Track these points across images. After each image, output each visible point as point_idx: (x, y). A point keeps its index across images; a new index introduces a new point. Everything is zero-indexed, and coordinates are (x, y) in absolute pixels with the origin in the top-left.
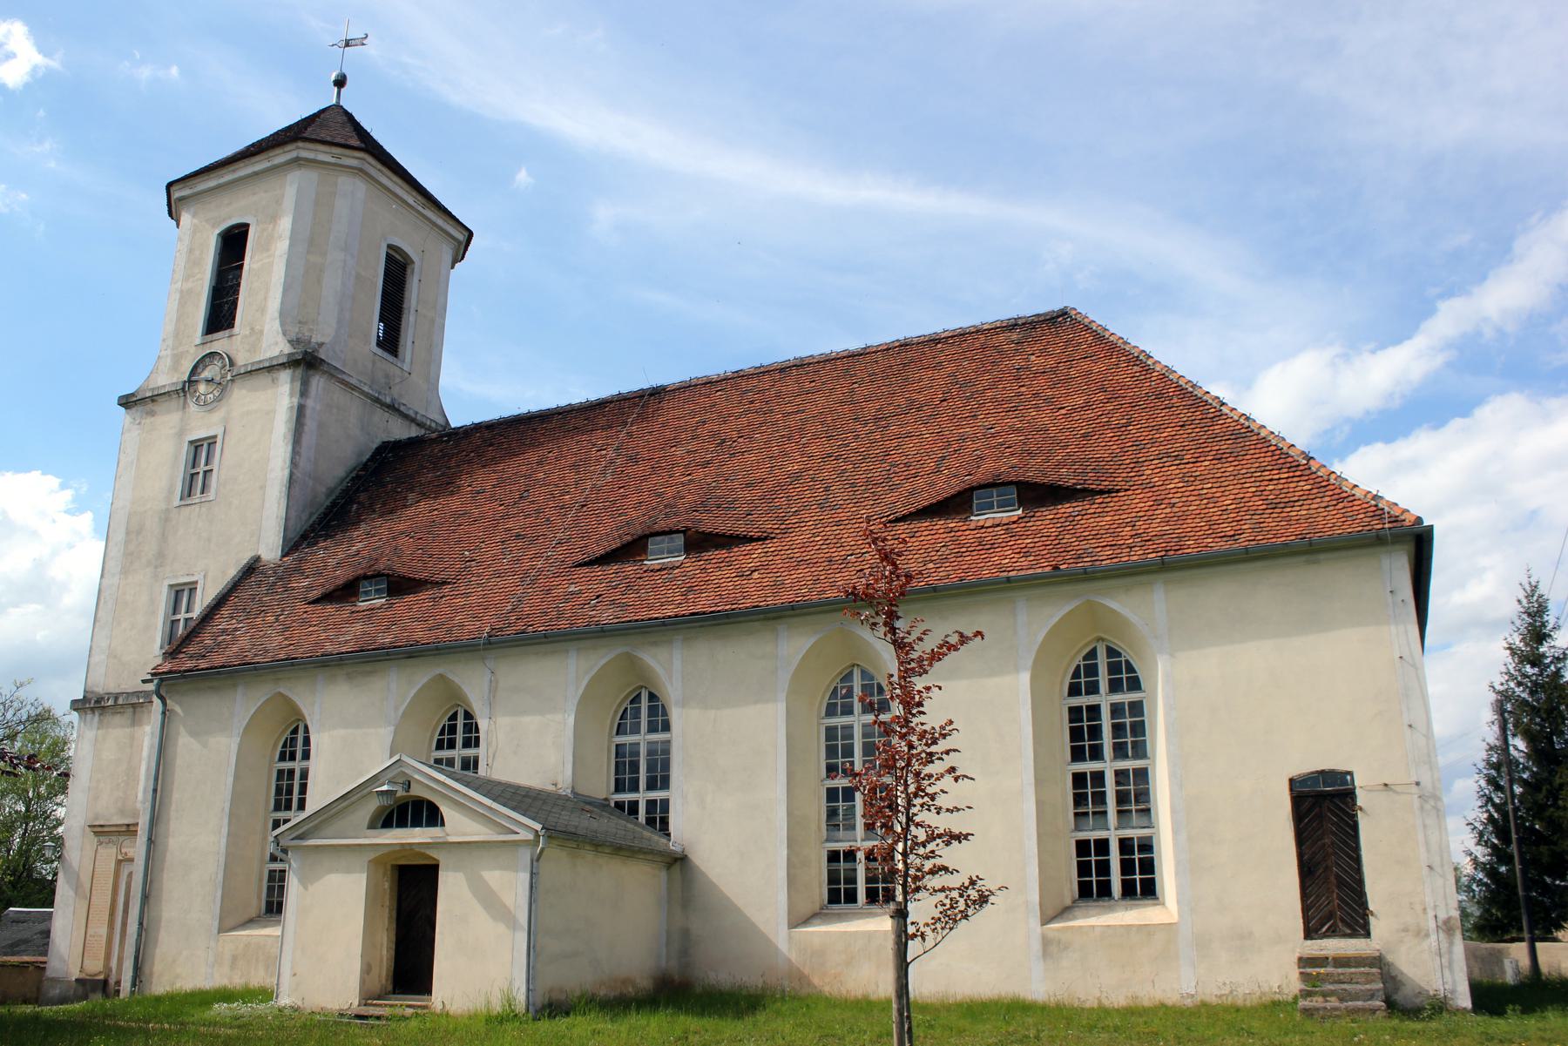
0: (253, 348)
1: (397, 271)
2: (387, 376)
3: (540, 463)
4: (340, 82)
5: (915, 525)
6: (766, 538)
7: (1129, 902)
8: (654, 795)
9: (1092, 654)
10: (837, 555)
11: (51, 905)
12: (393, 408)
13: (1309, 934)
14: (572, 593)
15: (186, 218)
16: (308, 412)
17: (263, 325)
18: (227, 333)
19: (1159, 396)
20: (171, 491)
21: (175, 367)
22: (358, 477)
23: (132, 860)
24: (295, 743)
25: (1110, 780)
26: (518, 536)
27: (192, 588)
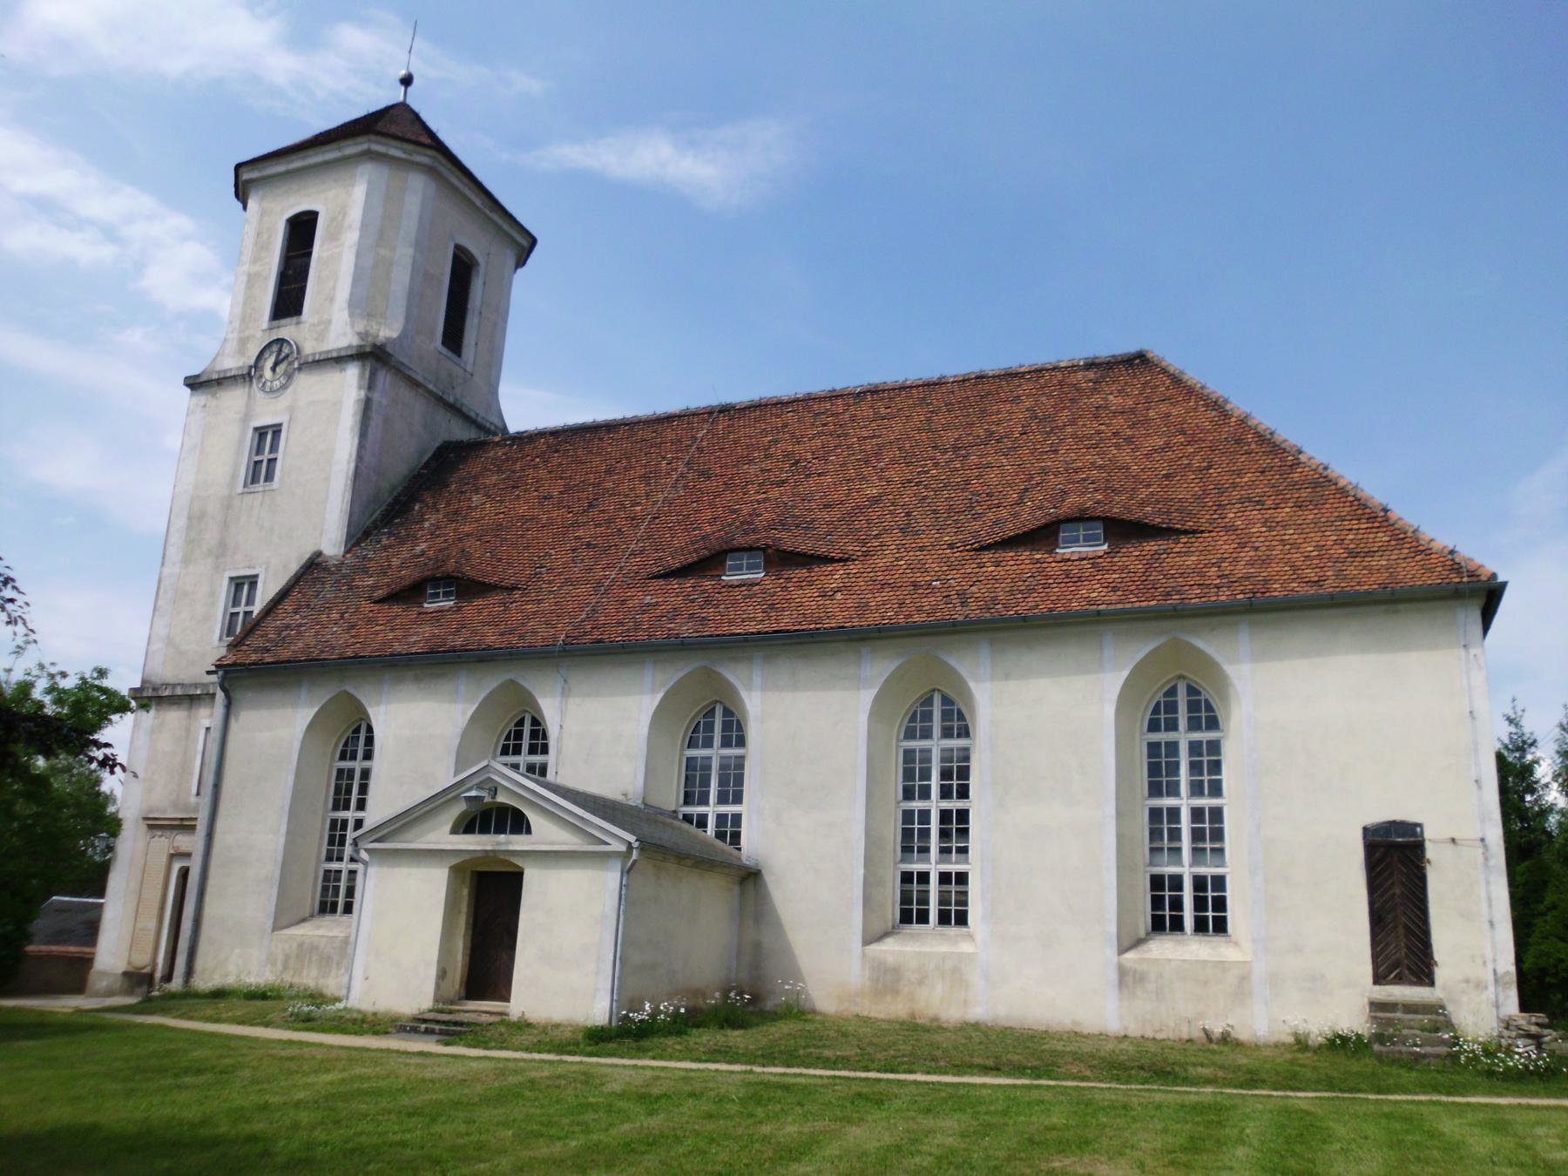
0: (321, 336)
1: (463, 269)
2: (450, 375)
3: (609, 472)
4: (407, 81)
5: (1000, 555)
6: (847, 560)
7: (1201, 938)
8: (724, 809)
9: (1172, 692)
10: (921, 579)
11: (101, 892)
12: (456, 410)
13: (1379, 979)
14: (649, 605)
15: (251, 203)
16: (374, 406)
17: (331, 317)
18: (295, 319)
19: (1239, 441)
20: (234, 477)
21: (242, 349)
22: (419, 475)
23: (188, 855)
24: (356, 739)
25: (1185, 816)
26: (588, 545)
27: (253, 581)
